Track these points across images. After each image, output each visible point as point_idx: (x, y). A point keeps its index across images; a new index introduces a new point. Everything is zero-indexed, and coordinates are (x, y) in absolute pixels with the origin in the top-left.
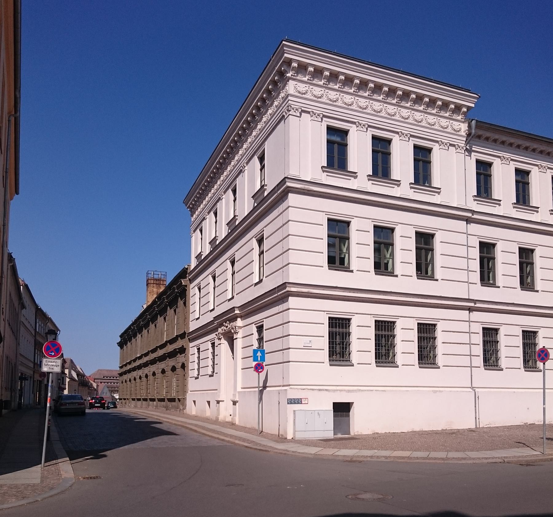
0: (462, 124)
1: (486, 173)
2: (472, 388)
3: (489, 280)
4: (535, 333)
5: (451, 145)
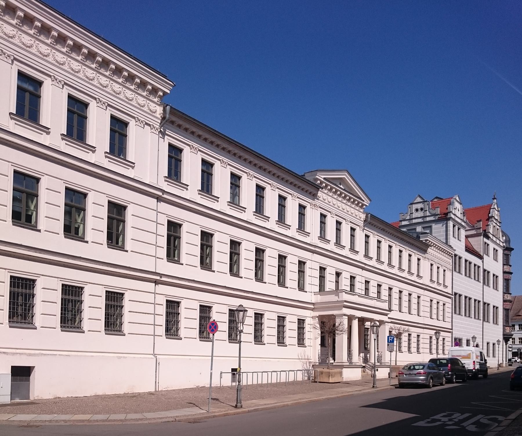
0: (157, 107)
1: (121, 132)
2: (154, 355)
3: (174, 257)
4: (210, 307)
5: (146, 124)
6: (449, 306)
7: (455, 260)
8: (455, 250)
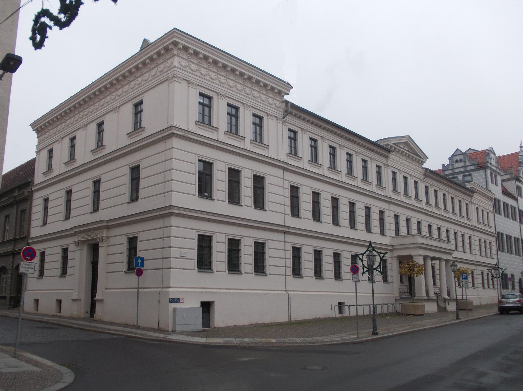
6: (494, 244)
7: (495, 203)
8: (494, 194)
